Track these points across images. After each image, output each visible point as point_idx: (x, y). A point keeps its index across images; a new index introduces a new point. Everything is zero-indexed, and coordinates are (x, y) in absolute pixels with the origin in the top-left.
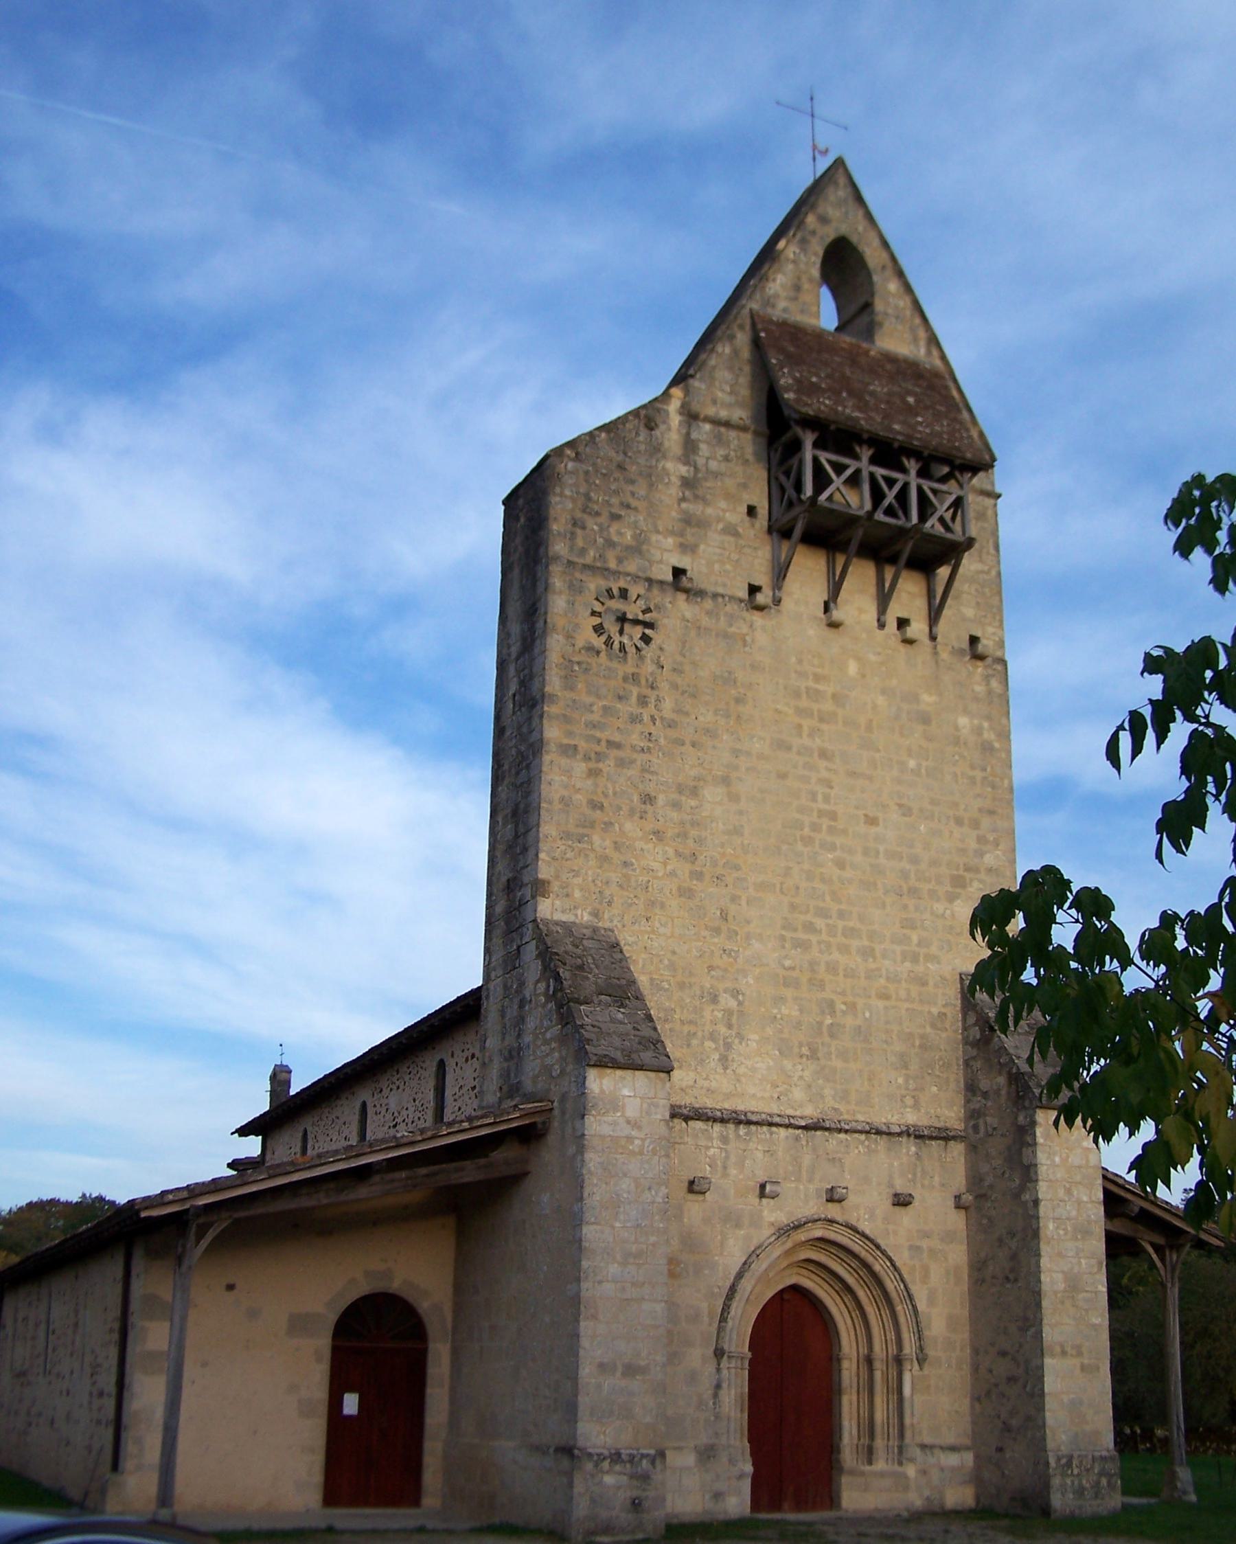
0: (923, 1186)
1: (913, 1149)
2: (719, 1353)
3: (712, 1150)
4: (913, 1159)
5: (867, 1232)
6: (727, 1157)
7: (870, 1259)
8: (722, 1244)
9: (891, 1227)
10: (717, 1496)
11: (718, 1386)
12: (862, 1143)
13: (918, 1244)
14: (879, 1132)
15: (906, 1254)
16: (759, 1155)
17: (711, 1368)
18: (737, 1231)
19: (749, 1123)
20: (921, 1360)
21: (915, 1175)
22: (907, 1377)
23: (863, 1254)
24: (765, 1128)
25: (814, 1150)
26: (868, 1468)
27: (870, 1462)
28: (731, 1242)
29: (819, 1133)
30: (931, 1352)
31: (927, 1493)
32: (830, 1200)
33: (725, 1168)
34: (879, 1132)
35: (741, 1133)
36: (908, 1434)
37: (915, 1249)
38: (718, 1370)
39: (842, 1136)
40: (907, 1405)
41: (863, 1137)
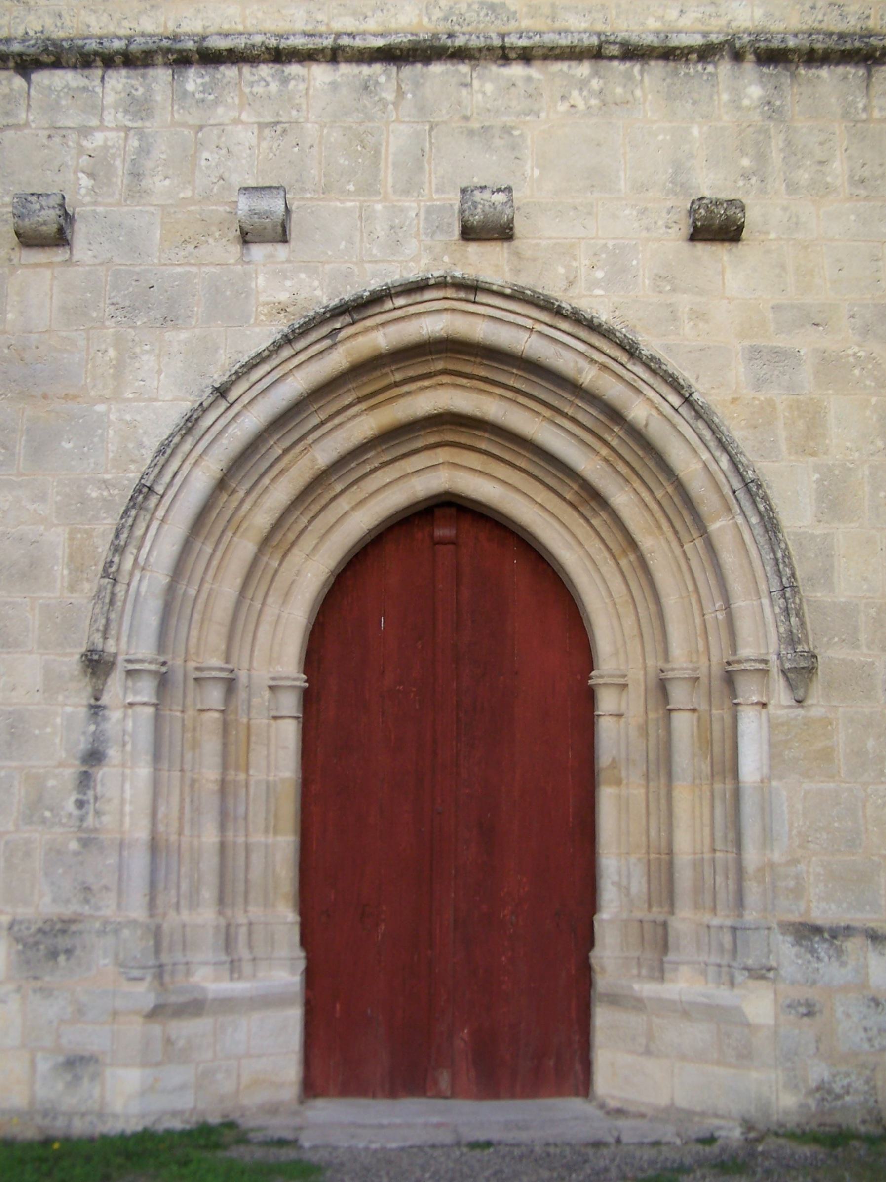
0: (792, 187)
1: (755, 92)
2: (96, 665)
3: (99, 138)
4: (756, 117)
5: (604, 316)
6: (144, 150)
7: (613, 390)
8: (119, 367)
9: (684, 301)
10: (76, 1064)
11: (94, 757)
12: (583, 84)
13: (781, 342)
14: (633, 53)
15: (739, 372)
16: (246, 136)
17: (74, 703)
18: (169, 335)
19: (210, 58)
20: (802, 673)
21: (761, 158)
22: (751, 725)
23: (588, 376)
24: (265, 70)
25: (422, 109)
26: (646, 989)
27: (660, 973)
28: (148, 361)
29: (437, 68)
30: (832, 654)
31: (818, 1072)
32: (470, 233)
33: (136, 175)
34: (633, 53)
35: (190, 87)
36: (753, 892)
37: (770, 360)
38: (96, 710)
39: (517, 70)
40: (749, 807)
41: (584, 69)
